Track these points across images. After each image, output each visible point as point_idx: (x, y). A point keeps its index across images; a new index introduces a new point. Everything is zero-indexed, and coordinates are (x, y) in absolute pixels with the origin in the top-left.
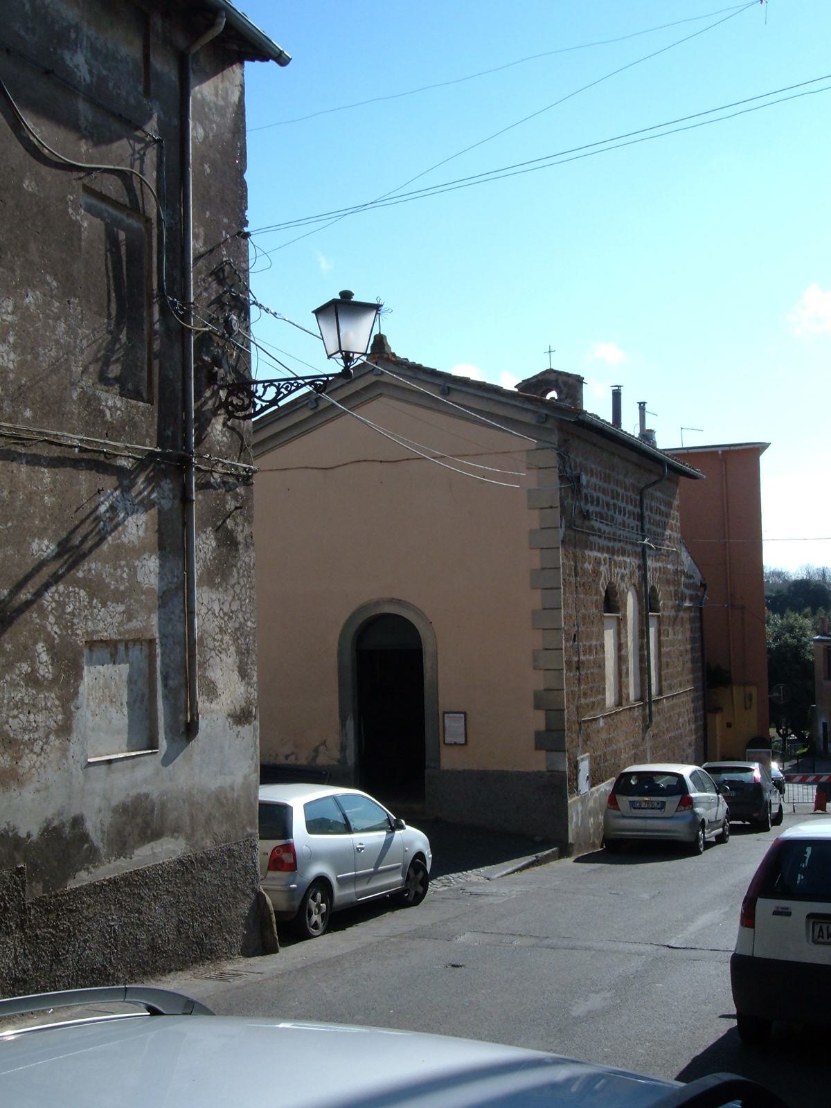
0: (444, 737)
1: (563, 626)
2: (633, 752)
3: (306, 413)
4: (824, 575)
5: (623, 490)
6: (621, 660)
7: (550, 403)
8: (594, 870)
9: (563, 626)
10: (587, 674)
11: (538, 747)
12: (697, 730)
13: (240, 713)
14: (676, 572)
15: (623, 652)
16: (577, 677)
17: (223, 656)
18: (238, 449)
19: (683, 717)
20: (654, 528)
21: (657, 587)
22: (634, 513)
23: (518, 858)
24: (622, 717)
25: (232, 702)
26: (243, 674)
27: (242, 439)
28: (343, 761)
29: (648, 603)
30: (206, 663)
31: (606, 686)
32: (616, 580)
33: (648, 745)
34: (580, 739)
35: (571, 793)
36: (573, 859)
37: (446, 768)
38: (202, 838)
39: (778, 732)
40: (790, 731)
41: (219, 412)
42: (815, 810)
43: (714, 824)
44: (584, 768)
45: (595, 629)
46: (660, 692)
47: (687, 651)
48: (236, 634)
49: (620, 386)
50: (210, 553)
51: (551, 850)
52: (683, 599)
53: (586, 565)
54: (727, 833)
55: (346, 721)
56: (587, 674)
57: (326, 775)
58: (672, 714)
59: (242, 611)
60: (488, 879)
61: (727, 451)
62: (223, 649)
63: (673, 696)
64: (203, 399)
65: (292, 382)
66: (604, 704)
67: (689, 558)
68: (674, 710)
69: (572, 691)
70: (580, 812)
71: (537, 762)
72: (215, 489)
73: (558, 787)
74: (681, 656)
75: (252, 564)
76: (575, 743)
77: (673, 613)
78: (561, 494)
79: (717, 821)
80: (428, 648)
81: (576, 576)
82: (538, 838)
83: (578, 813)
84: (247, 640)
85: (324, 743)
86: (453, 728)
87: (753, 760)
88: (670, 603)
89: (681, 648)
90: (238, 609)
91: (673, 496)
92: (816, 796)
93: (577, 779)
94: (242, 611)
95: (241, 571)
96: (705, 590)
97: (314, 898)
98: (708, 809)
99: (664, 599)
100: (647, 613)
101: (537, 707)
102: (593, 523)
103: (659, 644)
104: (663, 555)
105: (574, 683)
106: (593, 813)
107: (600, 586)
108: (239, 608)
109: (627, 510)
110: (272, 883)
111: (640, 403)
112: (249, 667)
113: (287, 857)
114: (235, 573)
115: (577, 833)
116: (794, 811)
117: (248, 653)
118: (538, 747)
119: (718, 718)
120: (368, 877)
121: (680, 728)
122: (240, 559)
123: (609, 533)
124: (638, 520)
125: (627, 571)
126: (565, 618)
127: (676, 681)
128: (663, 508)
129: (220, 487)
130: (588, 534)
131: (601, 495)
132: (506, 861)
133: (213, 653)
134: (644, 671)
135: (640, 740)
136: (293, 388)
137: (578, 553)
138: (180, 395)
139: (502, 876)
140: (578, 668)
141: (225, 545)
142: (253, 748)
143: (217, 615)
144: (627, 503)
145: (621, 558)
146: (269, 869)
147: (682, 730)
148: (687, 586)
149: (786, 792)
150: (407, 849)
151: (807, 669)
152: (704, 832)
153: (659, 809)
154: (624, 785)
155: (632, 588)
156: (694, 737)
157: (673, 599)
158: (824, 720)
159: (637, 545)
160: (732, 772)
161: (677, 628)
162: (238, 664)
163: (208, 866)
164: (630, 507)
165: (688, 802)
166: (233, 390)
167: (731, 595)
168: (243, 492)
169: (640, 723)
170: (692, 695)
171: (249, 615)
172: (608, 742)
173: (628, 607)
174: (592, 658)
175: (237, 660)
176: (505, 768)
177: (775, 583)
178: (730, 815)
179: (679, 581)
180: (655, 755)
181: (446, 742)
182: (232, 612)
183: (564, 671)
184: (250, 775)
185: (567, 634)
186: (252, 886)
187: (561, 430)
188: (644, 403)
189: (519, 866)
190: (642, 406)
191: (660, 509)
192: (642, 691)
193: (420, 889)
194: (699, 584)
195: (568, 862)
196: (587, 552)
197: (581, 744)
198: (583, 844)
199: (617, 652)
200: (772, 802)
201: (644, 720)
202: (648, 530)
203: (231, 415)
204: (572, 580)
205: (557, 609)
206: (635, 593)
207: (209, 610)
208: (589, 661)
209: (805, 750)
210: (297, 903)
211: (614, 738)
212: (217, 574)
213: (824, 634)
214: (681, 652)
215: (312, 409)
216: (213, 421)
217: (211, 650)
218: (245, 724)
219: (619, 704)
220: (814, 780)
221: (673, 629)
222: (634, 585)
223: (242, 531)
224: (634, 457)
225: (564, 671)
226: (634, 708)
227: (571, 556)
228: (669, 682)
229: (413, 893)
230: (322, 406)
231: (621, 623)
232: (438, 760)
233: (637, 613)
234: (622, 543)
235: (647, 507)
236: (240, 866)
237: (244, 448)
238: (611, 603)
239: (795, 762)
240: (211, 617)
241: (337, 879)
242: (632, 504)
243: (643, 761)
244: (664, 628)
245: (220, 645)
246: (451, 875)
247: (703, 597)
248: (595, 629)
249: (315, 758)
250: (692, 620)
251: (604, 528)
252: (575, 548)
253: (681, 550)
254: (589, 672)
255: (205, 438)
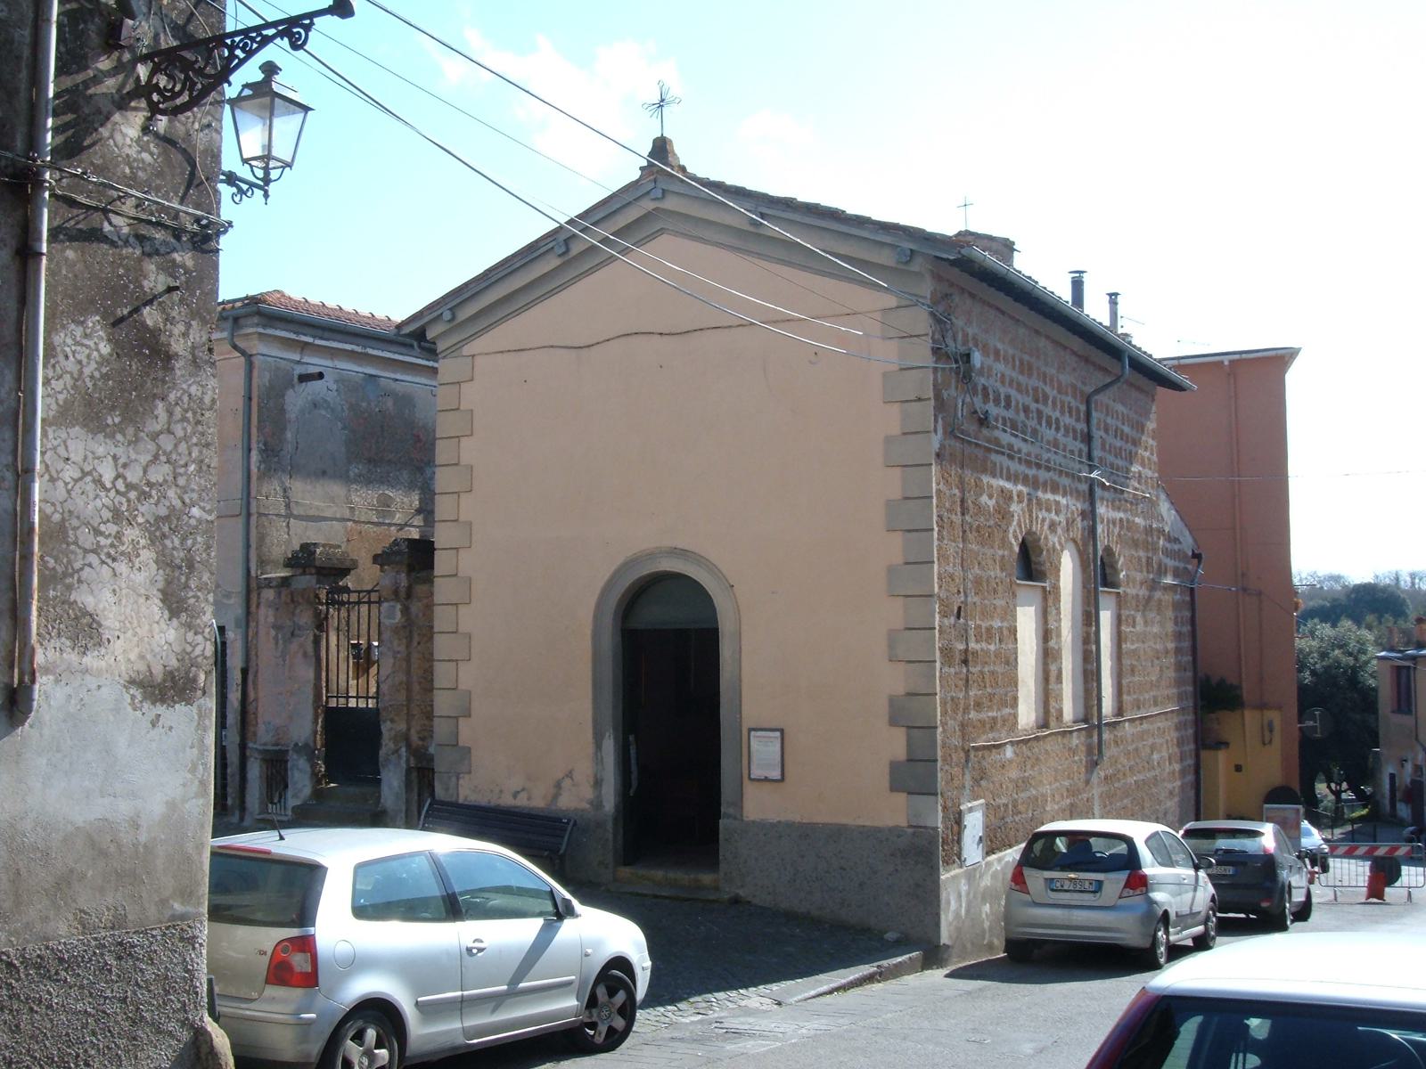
0: (749, 767)
1: (936, 590)
2: (1068, 801)
3: (552, 262)
4: (1397, 579)
5: (1055, 392)
6: (1048, 655)
7: (966, 281)
8: (969, 993)
9: (936, 590)
10: (981, 672)
11: (894, 788)
12: (1183, 772)
13: (165, 681)
14: (1149, 530)
15: (1052, 643)
16: (963, 676)
17: (122, 567)
18: (180, 180)
19: (1160, 752)
20: (1110, 458)
21: (1116, 549)
22: (1075, 431)
23: (845, 968)
24: (1049, 745)
25: (142, 657)
26: (174, 604)
27: (193, 166)
28: (597, 804)
29: (1100, 574)
30: (72, 576)
31: (1020, 694)
32: (1042, 530)
33: (1096, 792)
34: (968, 777)
35: (947, 863)
36: (946, 971)
37: (752, 818)
38: (45, 919)
39: (1329, 787)
40: (1345, 785)
41: (133, 104)
42: (1368, 898)
43: (1186, 919)
44: (974, 824)
45: (1000, 603)
46: (1120, 711)
47: (1167, 652)
48: (159, 528)
49: (1083, 272)
50: (93, 365)
51: (907, 956)
52: (1162, 571)
53: (984, 499)
54: (1213, 933)
55: (602, 739)
56: (981, 672)
57: (568, 823)
58: (1140, 746)
59: (177, 486)
60: (779, 1004)
61: (1238, 360)
62: (123, 553)
63: (1141, 718)
64: (91, 73)
65: (254, 35)
66: (1016, 723)
67: (1173, 512)
68: (1143, 740)
69: (952, 699)
70: (963, 893)
71: (892, 811)
72: (113, 244)
73: (924, 853)
74: (1158, 658)
75: (207, 400)
76: (956, 783)
77: (1143, 592)
78: (935, 379)
79: (1193, 915)
80: (726, 626)
81: (963, 514)
82: (890, 936)
83: (960, 896)
84: (190, 542)
85: (570, 775)
86: (763, 753)
87: (1260, 818)
88: (1139, 576)
89: (1158, 647)
90: (165, 481)
91: (1146, 414)
92: (1370, 877)
93: (959, 841)
94: (177, 486)
95: (178, 410)
96: (1199, 562)
97: (359, 1037)
98: (1174, 895)
99: (1128, 569)
100: (1096, 589)
101: (893, 722)
102: (997, 433)
103: (1119, 639)
104: (1126, 501)
105: (956, 686)
106: (987, 896)
107: (1011, 536)
108: (170, 478)
109: (1062, 424)
110: (268, 1008)
111: (1110, 295)
112: (191, 594)
113: (299, 962)
114: (160, 408)
115: (959, 930)
116: (1336, 899)
117: (191, 566)
118: (894, 788)
119: (1221, 755)
120: (496, 1001)
121: (1153, 768)
122: (174, 386)
123: (1029, 454)
124: (1082, 442)
125: (1062, 518)
126: (940, 578)
127: (1147, 696)
128: (1126, 429)
129: (126, 243)
130: (989, 450)
131: (1013, 393)
132: (822, 972)
133: (92, 558)
134: (1090, 674)
135: (1081, 785)
136: (255, 46)
137: (969, 476)
138: (26, 52)
139: (806, 999)
140: (965, 662)
141: (137, 354)
142: (195, 751)
143: (109, 485)
144: (1062, 413)
145: (1049, 496)
146: (268, 981)
147: (1157, 772)
148: (1167, 553)
149: (1331, 870)
150: (589, 951)
151: (1368, 700)
152: (1167, 932)
153: (1092, 892)
154: (1042, 853)
155: (1071, 545)
156: (1178, 783)
157: (1145, 569)
158: (1391, 770)
159: (1079, 479)
160: (1234, 837)
161: (1151, 615)
162: (161, 585)
163: (57, 973)
164: (1067, 420)
165: (1139, 882)
166: (160, 64)
167: (1243, 575)
168: (190, 263)
169: (1081, 756)
170: (1176, 720)
171: (195, 496)
172: (1024, 783)
173: (1062, 574)
174: (992, 647)
175: (159, 578)
176: (844, 820)
177: (1331, 590)
178: (1219, 904)
179: (1155, 544)
180: (1108, 808)
181: (752, 777)
182: (149, 484)
183: (938, 665)
184: (184, 801)
185: (945, 604)
186: (181, 1016)
187: (938, 278)
188: (1116, 294)
189: (844, 981)
190: (1113, 297)
191: (1122, 431)
192: (1087, 707)
193: (619, 1023)
194: (1190, 554)
195: (936, 975)
196: (986, 479)
197: (968, 782)
198: (969, 946)
199: (1041, 642)
200: (1293, 884)
201: (1089, 751)
202: (1101, 458)
203: (154, 109)
204: (957, 519)
205: (928, 562)
206: (1075, 551)
207: (85, 474)
208: (987, 652)
209: (1364, 812)
210: (315, 1048)
211: (1034, 778)
212: (113, 408)
213: (1392, 649)
214: (1157, 651)
215: (560, 256)
216: (117, 117)
217: (86, 551)
218: (175, 702)
219: (1044, 724)
220: (1366, 853)
221: (1144, 616)
222: (1074, 541)
223: (185, 335)
224: (1076, 343)
225: (938, 665)
226: (1071, 732)
227: (954, 480)
228: (1135, 697)
229: (603, 1029)
230: (576, 249)
231: (1048, 602)
232: (739, 802)
233: (1079, 585)
234: (1051, 473)
235: (1098, 424)
236: (149, 976)
237: (196, 182)
238: (1032, 564)
239: (1349, 828)
240: (90, 487)
241: (417, 1003)
242: (1071, 416)
243: (1088, 814)
244: (1128, 613)
245: (112, 545)
246: (716, 994)
247: (1197, 571)
248: (1000, 603)
249: (556, 796)
250: (1176, 606)
251: (1017, 444)
252: (962, 467)
253: (1158, 497)
254: (986, 669)
255: (90, 146)
